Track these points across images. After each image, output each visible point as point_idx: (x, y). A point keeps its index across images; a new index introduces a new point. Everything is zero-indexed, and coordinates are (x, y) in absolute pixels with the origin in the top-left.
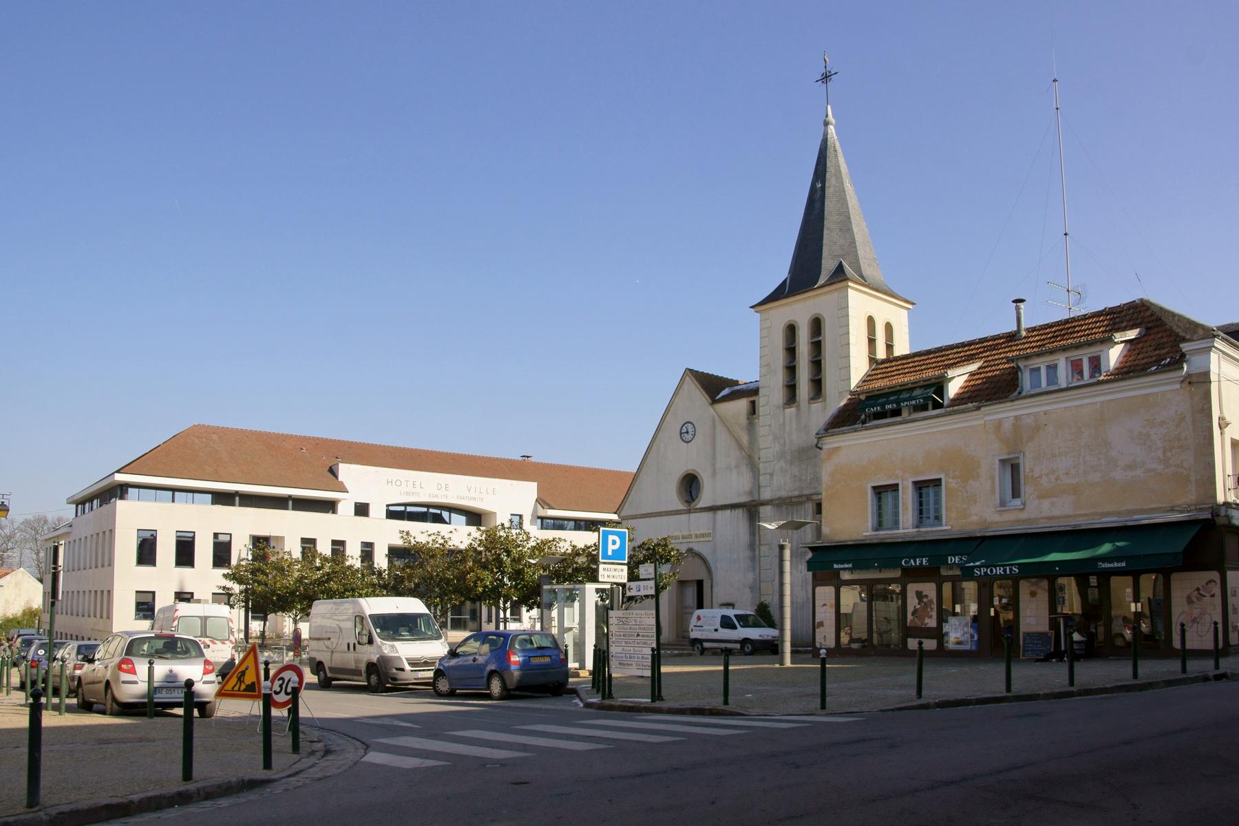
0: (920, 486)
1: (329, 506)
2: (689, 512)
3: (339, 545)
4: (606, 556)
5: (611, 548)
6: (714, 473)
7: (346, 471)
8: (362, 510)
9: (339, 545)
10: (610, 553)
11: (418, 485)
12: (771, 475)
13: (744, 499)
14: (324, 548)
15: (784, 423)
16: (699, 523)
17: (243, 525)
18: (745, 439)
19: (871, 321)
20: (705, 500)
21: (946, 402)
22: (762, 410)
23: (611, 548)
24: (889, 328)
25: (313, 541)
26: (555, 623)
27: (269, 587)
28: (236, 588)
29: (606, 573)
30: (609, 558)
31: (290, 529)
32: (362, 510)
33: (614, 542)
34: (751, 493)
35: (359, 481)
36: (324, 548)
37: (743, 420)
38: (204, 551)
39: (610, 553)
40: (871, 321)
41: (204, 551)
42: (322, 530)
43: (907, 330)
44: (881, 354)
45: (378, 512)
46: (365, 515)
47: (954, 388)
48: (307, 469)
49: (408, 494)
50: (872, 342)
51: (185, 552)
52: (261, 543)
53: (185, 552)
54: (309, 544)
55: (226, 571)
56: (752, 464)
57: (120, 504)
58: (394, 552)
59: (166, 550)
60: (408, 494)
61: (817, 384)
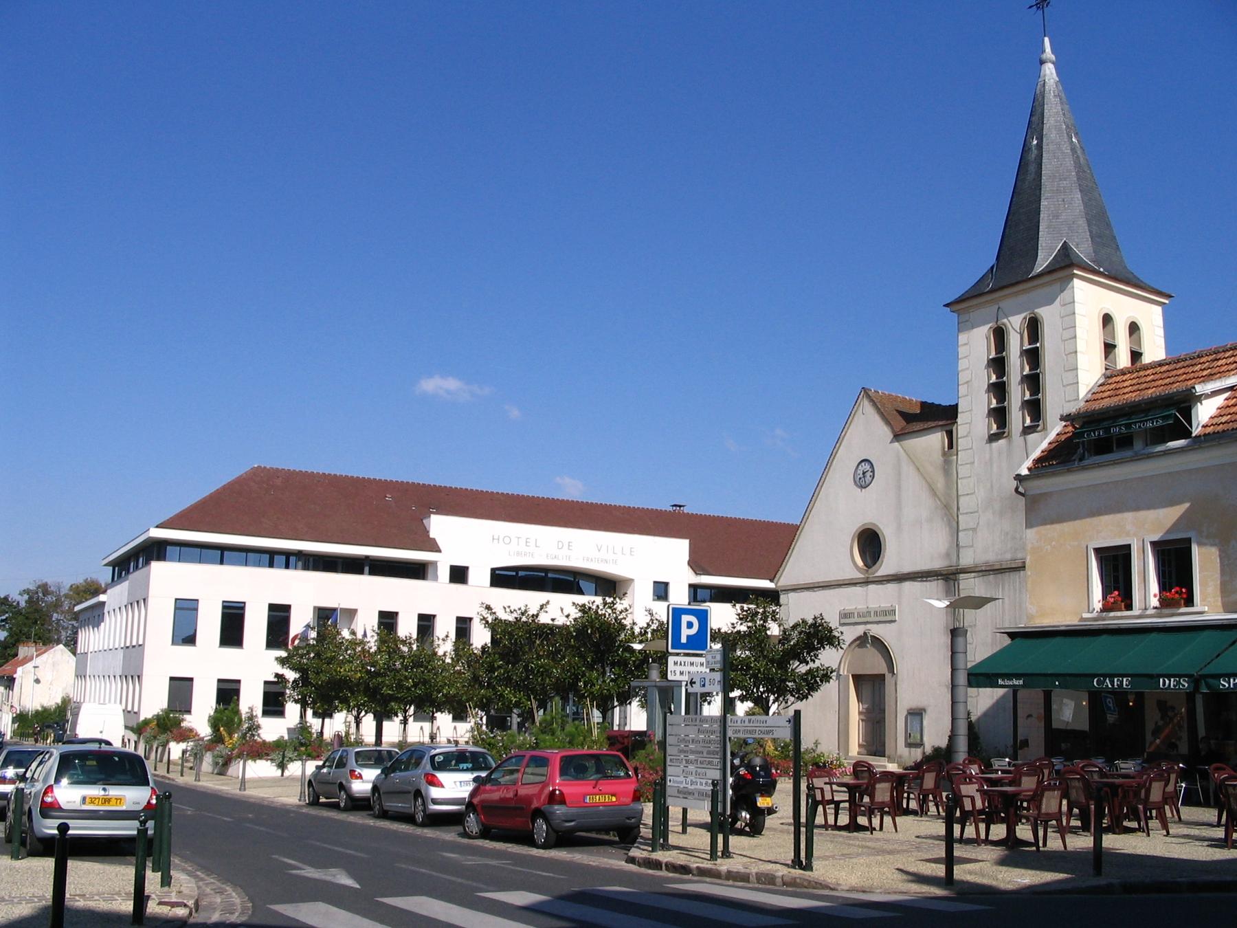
0: (190, 640)
1: (417, 571)
2: (866, 582)
3: (426, 623)
4: (677, 644)
5: (685, 633)
6: (899, 528)
7: (440, 526)
8: (459, 575)
9: (426, 623)
10: (684, 640)
11: (532, 543)
12: (974, 530)
13: (937, 564)
14: (407, 628)
15: (991, 459)
16: (878, 597)
17: (306, 593)
18: (940, 483)
19: (1107, 320)
20: (887, 566)
21: (1196, 431)
22: (962, 443)
23: (685, 633)
24: (1134, 328)
25: (394, 615)
26: (417, 732)
27: (326, 671)
28: (291, 675)
29: (678, 669)
30: (684, 646)
31: (364, 599)
32: (459, 575)
33: (690, 625)
34: (948, 555)
35: (456, 538)
36: (407, 628)
37: (938, 457)
38: (256, 626)
39: (684, 640)
40: (1107, 320)
41: (256, 626)
42: (407, 599)
43: (1161, 332)
44: (1123, 359)
45: (479, 576)
46: (464, 579)
47: (1205, 412)
48: (382, 521)
49: (518, 554)
50: (1109, 348)
51: (232, 630)
52: (324, 615)
53: (232, 630)
54: (388, 620)
55: (283, 654)
56: (949, 510)
57: (156, 566)
58: (496, 626)
59: (209, 624)
60: (518, 554)
61: (1034, 408)
